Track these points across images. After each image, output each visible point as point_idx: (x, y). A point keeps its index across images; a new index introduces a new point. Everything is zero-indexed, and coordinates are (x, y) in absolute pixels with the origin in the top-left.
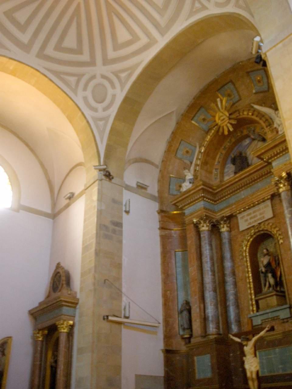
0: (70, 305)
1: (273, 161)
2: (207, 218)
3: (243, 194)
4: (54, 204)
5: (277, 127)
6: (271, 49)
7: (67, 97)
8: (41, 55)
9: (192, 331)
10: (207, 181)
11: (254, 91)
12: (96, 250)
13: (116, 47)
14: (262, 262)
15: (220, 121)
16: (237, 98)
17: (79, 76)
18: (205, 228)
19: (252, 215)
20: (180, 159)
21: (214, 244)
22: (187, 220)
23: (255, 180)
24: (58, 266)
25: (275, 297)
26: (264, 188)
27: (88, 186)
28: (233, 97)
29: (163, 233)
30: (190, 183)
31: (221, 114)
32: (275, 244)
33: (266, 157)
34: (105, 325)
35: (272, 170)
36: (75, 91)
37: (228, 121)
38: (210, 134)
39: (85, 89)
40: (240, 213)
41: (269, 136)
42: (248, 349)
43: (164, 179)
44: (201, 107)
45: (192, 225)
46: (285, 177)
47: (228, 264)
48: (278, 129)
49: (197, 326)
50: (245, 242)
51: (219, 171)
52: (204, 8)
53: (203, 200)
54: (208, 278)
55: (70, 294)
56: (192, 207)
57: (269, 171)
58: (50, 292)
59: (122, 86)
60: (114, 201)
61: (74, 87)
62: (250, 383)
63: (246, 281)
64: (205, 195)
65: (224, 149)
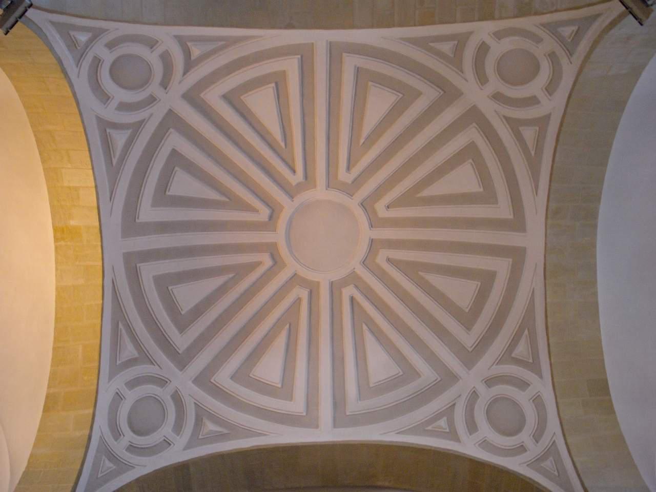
8: (133, 262)
13: (242, 376)
17: (144, 357)
36: (115, 370)
39: (133, 384)
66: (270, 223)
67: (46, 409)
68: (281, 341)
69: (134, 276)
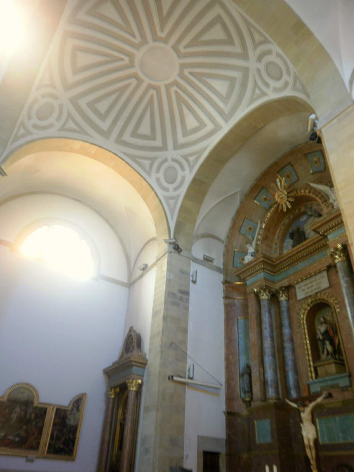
0: (139, 365)
1: (328, 234)
2: (266, 288)
3: (300, 266)
4: (130, 274)
5: (333, 202)
6: (325, 125)
7: (142, 179)
8: (119, 141)
9: (252, 394)
10: (268, 254)
11: (311, 172)
12: (164, 315)
13: (186, 133)
14: (320, 330)
15: (279, 200)
16: (295, 178)
18: (264, 297)
19: (309, 285)
20: (244, 235)
21: (273, 312)
22: (248, 290)
23: (311, 253)
24: (131, 329)
25: (333, 365)
26: (321, 260)
27: (159, 258)
28: (292, 177)
29: (227, 302)
30: (252, 256)
31: (280, 193)
32: (332, 313)
33: (321, 231)
34: (170, 385)
35: (328, 243)
36: (149, 173)
38: (270, 212)
39: (158, 171)
40: (298, 283)
41: (325, 211)
42: (306, 415)
43: (229, 253)
44: (263, 188)
45: (253, 295)
46: (340, 249)
47: (286, 331)
48: (333, 204)
49: (256, 389)
50: (303, 311)
51: (278, 245)
52: (264, 94)
53: (264, 271)
54: (267, 343)
55: (139, 356)
56: (253, 278)
57: (325, 243)
58: (123, 353)
60: (182, 272)
61: (148, 170)
62: (308, 451)
63: (304, 347)
64: (265, 267)
65: (283, 225)
66: (140, 81)
69: (125, 144)
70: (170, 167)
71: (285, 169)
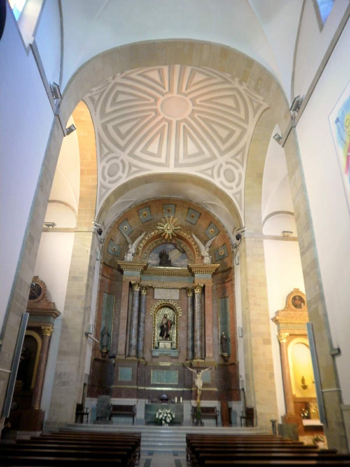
13: (144, 151)
17: (111, 151)
30: (132, 255)
36: (102, 159)
37: (171, 232)
39: (107, 162)
59: (129, 174)
61: (103, 156)
67: (81, 174)
68: (158, 139)
70: (117, 164)
71: (170, 206)
